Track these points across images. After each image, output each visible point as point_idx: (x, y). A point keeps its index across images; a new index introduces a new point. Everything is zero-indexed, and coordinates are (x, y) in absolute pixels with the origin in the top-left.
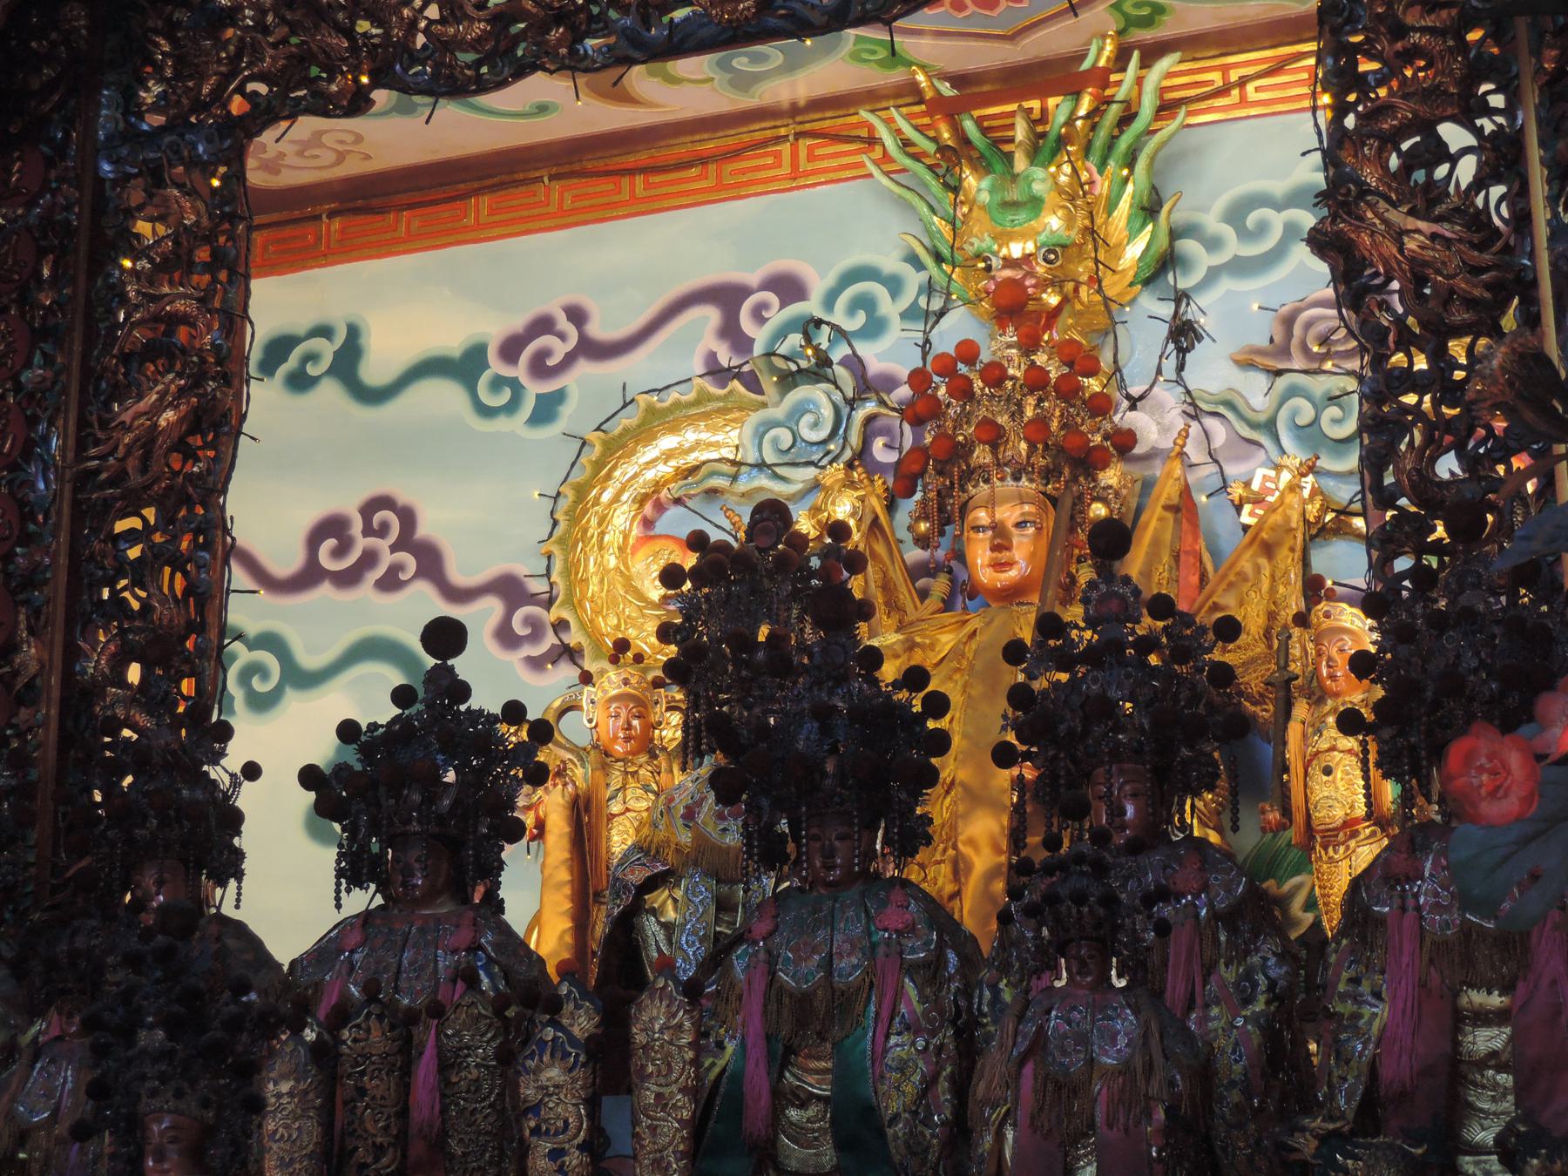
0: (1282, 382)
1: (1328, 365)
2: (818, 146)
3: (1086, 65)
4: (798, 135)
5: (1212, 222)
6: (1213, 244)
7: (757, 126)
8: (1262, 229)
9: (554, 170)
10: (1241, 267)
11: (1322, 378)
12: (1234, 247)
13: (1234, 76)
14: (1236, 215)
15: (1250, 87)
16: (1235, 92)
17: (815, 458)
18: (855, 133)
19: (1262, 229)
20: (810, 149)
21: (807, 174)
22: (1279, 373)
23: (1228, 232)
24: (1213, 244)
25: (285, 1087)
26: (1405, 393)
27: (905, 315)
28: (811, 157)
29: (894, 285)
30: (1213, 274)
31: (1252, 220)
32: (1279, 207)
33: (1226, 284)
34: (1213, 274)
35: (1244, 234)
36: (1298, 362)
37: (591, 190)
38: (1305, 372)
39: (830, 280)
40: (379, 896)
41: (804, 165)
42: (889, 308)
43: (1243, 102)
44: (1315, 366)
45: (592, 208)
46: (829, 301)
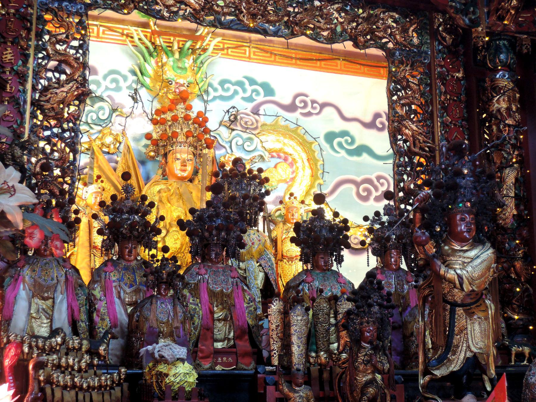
0: (234, 133)
1: (248, 131)
2: (258, 52)
3: (198, 34)
4: (101, 26)
5: (216, 84)
6: (215, 90)
7: (267, 44)
8: (228, 89)
9: (344, 58)
10: (222, 98)
11: (246, 134)
12: (220, 92)
13: (226, 46)
14: (222, 83)
15: (230, 50)
16: (226, 51)
17: (101, 124)
18: (118, 30)
19: (228, 89)
20: (104, 31)
21: (102, 38)
22: (233, 130)
23: (219, 88)
24: (215, 90)
25: (299, 318)
26: (408, 158)
27: (128, 88)
28: (103, 33)
29: (125, 78)
30: (215, 98)
31: (226, 86)
32: (233, 84)
33: (218, 101)
34: (215, 98)
35: (223, 89)
36: (239, 128)
37: (353, 67)
38: (242, 131)
39: (106, 72)
40: (230, 264)
41: (101, 35)
42: (122, 83)
43: (227, 54)
44: (244, 130)
45: (327, 69)
46: (105, 77)
